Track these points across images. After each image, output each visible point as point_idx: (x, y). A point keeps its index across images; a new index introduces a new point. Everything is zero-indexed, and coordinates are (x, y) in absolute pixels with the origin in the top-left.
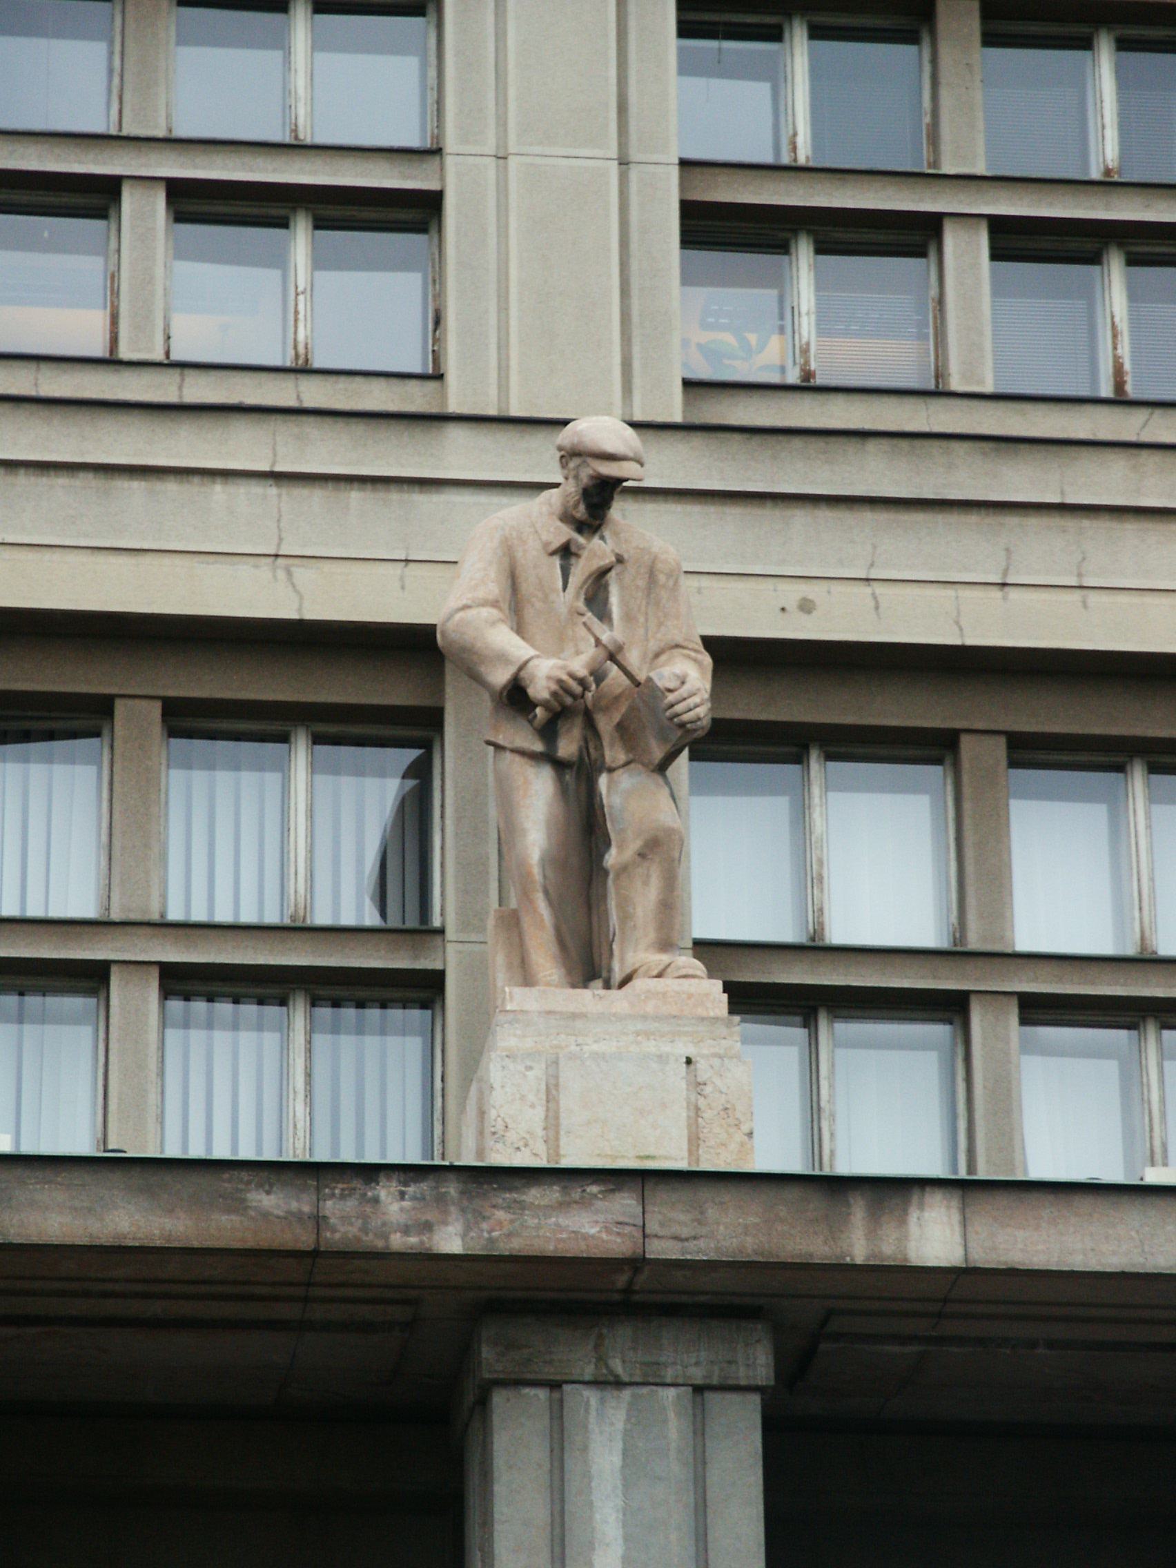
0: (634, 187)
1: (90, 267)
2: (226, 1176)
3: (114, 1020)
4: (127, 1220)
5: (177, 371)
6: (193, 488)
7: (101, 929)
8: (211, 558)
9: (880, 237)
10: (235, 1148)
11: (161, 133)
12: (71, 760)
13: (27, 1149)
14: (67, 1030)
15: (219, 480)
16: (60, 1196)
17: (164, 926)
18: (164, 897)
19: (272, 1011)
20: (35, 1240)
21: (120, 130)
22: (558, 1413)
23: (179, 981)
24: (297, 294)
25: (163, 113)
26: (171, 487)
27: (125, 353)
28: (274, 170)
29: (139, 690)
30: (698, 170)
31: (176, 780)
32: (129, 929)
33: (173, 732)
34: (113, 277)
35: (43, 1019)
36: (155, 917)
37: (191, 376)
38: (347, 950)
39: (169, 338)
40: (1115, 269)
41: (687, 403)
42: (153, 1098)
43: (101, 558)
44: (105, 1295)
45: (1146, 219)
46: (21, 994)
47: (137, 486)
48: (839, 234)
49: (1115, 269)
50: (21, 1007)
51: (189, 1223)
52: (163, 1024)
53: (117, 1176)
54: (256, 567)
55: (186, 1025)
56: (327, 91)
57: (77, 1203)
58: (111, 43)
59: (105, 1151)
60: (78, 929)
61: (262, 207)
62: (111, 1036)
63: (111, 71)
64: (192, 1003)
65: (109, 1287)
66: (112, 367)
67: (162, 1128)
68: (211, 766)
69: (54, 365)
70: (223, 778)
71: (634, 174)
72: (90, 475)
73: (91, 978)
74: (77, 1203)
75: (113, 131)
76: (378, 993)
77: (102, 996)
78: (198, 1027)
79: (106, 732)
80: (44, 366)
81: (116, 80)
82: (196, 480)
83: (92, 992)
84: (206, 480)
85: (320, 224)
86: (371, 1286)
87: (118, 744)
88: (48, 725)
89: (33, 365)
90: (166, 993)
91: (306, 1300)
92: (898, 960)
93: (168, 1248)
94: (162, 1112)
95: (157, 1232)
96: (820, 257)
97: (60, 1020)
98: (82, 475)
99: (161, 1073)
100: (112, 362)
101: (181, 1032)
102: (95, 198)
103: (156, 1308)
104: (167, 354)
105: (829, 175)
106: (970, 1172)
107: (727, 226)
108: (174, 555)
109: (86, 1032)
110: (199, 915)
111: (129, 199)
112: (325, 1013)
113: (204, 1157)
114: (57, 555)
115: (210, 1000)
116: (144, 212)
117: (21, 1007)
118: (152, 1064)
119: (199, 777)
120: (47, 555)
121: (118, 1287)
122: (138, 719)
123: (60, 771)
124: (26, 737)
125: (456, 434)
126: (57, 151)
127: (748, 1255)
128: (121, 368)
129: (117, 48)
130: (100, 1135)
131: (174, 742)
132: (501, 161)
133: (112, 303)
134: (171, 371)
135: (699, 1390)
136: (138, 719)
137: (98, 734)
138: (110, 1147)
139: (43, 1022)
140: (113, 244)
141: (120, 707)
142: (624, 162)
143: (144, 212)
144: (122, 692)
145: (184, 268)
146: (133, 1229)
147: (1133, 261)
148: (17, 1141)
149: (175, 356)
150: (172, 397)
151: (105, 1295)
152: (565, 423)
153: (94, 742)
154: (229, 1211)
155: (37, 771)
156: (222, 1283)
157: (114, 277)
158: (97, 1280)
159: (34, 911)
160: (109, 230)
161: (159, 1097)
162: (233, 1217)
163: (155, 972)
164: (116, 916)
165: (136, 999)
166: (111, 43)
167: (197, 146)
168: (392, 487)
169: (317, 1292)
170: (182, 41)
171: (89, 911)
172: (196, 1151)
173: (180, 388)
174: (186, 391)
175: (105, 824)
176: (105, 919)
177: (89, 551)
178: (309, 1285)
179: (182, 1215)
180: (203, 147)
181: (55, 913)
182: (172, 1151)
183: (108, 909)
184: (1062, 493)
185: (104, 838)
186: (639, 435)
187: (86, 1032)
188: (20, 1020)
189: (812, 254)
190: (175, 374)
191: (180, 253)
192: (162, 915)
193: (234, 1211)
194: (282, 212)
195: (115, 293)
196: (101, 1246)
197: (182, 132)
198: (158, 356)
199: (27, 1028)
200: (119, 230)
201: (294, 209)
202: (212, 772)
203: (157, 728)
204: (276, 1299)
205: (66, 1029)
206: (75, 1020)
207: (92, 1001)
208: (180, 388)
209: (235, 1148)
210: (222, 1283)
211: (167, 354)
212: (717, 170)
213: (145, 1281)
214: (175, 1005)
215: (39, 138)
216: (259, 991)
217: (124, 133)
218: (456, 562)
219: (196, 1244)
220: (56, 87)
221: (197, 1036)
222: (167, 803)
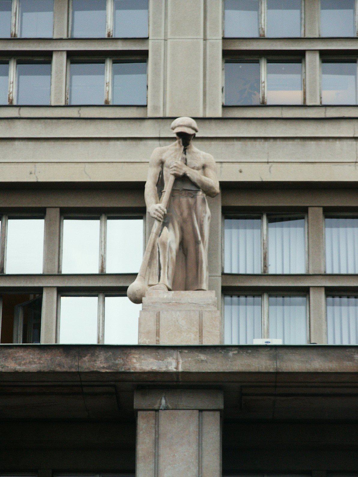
0: (208, 45)
1: (297, 77)
2: (347, 350)
3: (311, 304)
4: (318, 364)
5: (324, 108)
6: (330, 143)
7: (307, 277)
8: (336, 164)
9: (289, 58)
10: (349, 342)
11: (317, 36)
12: (296, 226)
13: (287, 343)
14: (297, 307)
15: (338, 140)
16: (298, 357)
17: (326, 275)
18: (325, 266)
19: (257, 299)
20: (291, 371)
21: (305, 36)
22: (157, 419)
23: (331, 292)
24: (10, 84)
25: (317, 31)
26: (323, 143)
27: (308, 103)
28: (352, 46)
29: (316, 204)
30: (228, 40)
31: (227, 232)
32: (316, 277)
33: (326, 217)
34: (304, 80)
35: (290, 304)
36: (323, 273)
37: (329, 109)
38: (45, 279)
39: (321, 98)
40: (109, 65)
41: (223, 110)
42: (324, 327)
43: (303, 165)
44: (312, 387)
45: (333, 49)
46: (283, 297)
47: (313, 143)
48: (23, 58)
49: (109, 65)
50: (283, 301)
51: (337, 365)
52: (327, 305)
53: (314, 351)
54: (350, 166)
55: (333, 305)
56: (108, 23)
57: (303, 359)
58: (301, 10)
59: (311, 344)
60: (300, 277)
61: (95, 58)
62: (311, 309)
63: (301, 18)
64: (277, 298)
65: (313, 384)
66: (305, 108)
67: (327, 337)
68: (338, 226)
69: (272, 108)
70: (342, 230)
71: (208, 42)
72: (299, 140)
73: (304, 292)
74: (303, 359)
75: (303, 37)
76: (281, 293)
77: (308, 297)
78: (250, 305)
79: (306, 217)
80: (284, 108)
81: (303, 21)
82: (331, 140)
83: (305, 296)
84: (334, 140)
85: (269, 61)
86: (328, 382)
87: (310, 221)
88: (289, 216)
89: (280, 108)
90: (327, 296)
91: (276, 387)
92: (91, 276)
93: (331, 373)
94: (327, 331)
95: (327, 368)
96: (228, 64)
97: (295, 304)
98: (296, 140)
99: (326, 320)
100: (304, 106)
101: (230, 307)
102: (297, 57)
103: (328, 391)
104: (321, 103)
105: (278, 40)
106: (56, 342)
107: (134, 57)
108: (324, 163)
109: (303, 308)
110: (336, 272)
111: (308, 57)
112: (273, 299)
113: (340, 345)
114: (290, 165)
115: (340, 297)
116: (313, 61)
117: (283, 301)
118: (324, 317)
119: (335, 230)
120: (287, 165)
121: (316, 384)
122: (315, 213)
123: (293, 230)
124: (282, 220)
125: (148, 123)
126: (286, 43)
127: (213, 370)
128: (307, 108)
129: (303, 11)
130: (308, 339)
131: (327, 220)
132: (205, 41)
133: (304, 88)
134: (322, 108)
135: (201, 411)
136: (315, 213)
137: (303, 218)
138: (312, 342)
139: (290, 305)
140: (304, 71)
141: (310, 210)
142: (205, 39)
143: (313, 61)
144: (311, 205)
145: (325, 76)
146: (320, 367)
147: (19, 63)
148: (284, 341)
149: (324, 103)
150: (323, 116)
151: (312, 387)
152: (175, 118)
153: (303, 220)
154: (349, 361)
155: (285, 230)
156: (347, 382)
157: (304, 81)
158: (310, 382)
159: (286, 272)
160: (302, 66)
161: (326, 327)
162: (350, 363)
163: (323, 290)
164: (311, 272)
165: (318, 298)
166: (301, 10)
167: (342, 40)
168: (235, 140)
169: (83, 383)
170: (322, 8)
171: (302, 271)
172: (338, 343)
173: (325, 113)
174: (327, 114)
175: (307, 245)
176: (308, 274)
177: (299, 163)
178: (276, 382)
179: (335, 362)
180: (329, 40)
181: (293, 272)
182: (331, 343)
183: (308, 271)
184: (160, 134)
185: (307, 250)
186: (196, 122)
187: (303, 308)
188: (283, 305)
189: (111, 64)
190: (323, 109)
191: (324, 72)
192: (325, 272)
193: (351, 361)
194: (7, 59)
195: (305, 85)
196: (310, 372)
197: (323, 36)
198: (318, 103)
199: (286, 307)
200: (305, 66)
201: (10, 58)
202: (338, 229)
203: (321, 216)
204: (290, 387)
205: (297, 307)
206: (300, 304)
207: (304, 299)
208: (325, 113)
209: (349, 342)
210: (347, 382)
211: (321, 103)
212: (236, 40)
213: (72, 381)
214: (330, 299)
215: (92, 40)
216: (340, 294)
217: (306, 37)
218: (148, 162)
219: (339, 371)
220: (37, 26)
221: (337, 308)
222: (325, 238)
